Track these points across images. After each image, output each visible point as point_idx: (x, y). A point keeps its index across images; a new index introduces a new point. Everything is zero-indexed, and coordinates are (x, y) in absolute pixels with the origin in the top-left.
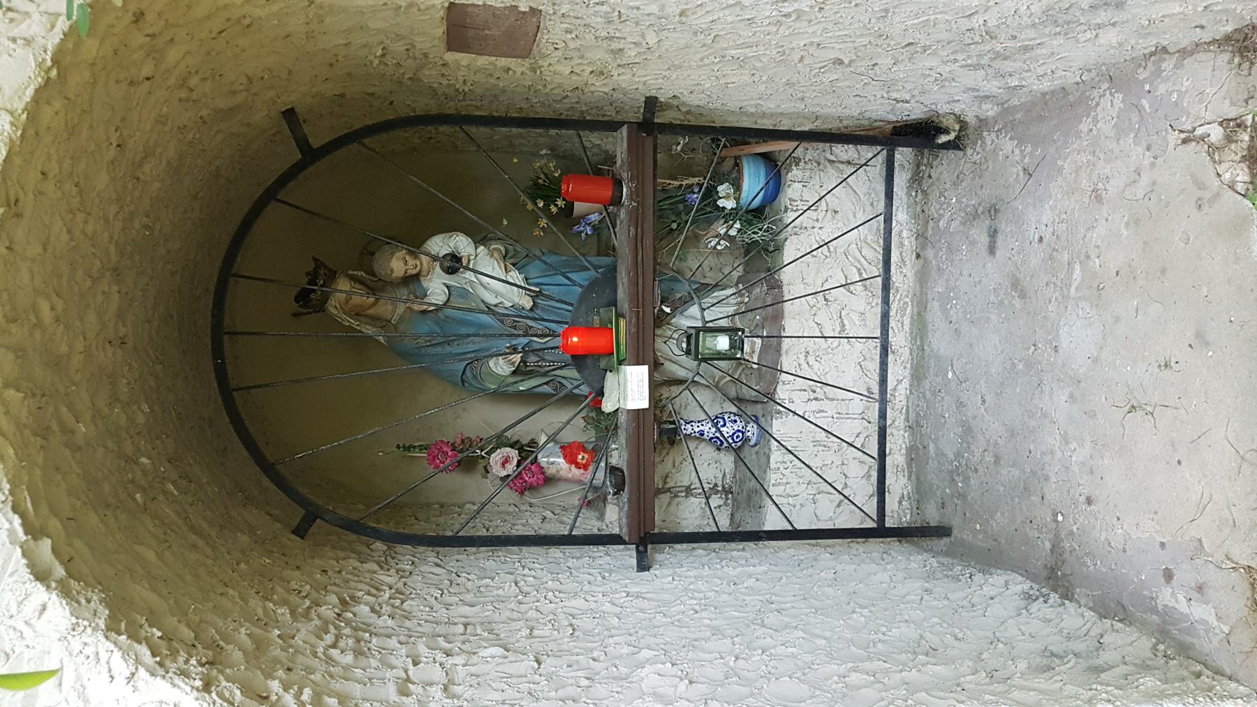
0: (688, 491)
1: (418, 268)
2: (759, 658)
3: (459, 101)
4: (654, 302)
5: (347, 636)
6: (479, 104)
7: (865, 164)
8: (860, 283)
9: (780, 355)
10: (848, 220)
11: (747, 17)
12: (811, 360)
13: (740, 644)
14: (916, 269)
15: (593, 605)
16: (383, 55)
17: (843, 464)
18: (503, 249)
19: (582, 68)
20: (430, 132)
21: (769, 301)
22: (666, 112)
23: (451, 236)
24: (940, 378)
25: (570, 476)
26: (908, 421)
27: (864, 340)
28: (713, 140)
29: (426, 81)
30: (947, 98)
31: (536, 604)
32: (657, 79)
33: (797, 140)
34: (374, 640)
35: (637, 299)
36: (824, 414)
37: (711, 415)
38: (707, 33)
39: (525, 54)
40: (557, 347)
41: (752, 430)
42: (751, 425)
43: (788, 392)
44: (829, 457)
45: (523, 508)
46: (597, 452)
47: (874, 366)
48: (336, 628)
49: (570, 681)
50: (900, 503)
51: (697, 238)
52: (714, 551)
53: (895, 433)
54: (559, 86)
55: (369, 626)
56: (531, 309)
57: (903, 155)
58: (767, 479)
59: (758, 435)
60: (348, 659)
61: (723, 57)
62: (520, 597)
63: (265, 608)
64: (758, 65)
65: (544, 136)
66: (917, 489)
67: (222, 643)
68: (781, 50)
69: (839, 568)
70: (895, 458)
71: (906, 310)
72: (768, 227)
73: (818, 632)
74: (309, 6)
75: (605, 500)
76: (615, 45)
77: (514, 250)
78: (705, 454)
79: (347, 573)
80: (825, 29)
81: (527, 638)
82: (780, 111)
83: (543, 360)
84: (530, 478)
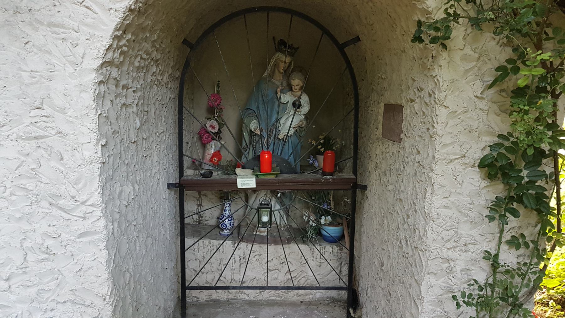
0: (200, 205)
1: (295, 91)
2: (135, 235)
3: (364, 108)
4: (282, 189)
5: (145, 63)
6: (363, 116)
7: (340, 278)
8: (290, 277)
9: (259, 244)
10: (317, 272)
11: (400, 226)
12: (257, 257)
13: (140, 227)
14: (296, 301)
15: (154, 165)
16: (382, 78)
17: (212, 272)
18: (303, 126)
19: (379, 159)
20: (351, 95)
21: (282, 239)
22: (361, 194)
23: (308, 104)
24: (250, 313)
25: (206, 154)
26: (231, 300)
27: (266, 280)
28: (350, 214)
29: (372, 95)
30: (368, 312)
31: (155, 141)
32: (374, 190)
33: (350, 249)
34: (143, 74)
35: (283, 182)
36: (234, 263)
37: (233, 215)
38: (393, 210)
39: (384, 136)
40: (263, 149)
41: (226, 232)
42: (229, 232)
43: (243, 247)
44: (215, 266)
45: (192, 134)
46: (217, 166)
47: (254, 284)
48: (148, 58)
49: (127, 156)
50: (195, 297)
51: (308, 208)
52: (175, 216)
53: (226, 294)
54: (371, 149)
55: (148, 72)
56: (278, 138)
57: (344, 294)
58: (206, 239)
59: (224, 235)
60: (137, 64)
61: (384, 217)
62: (158, 134)
63: (157, 30)
64: (381, 232)
65: (350, 143)
66: (202, 304)
67: (146, 15)
68: (387, 241)
69: (168, 270)
70: (215, 295)
71: (278, 297)
72: (313, 238)
73: (144, 260)
74: (401, 50)
75: (196, 169)
76: (388, 173)
77: (302, 131)
78: (216, 212)
79: (168, 61)
80: (396, 258)
81: (143, 137)
82: (362, 242)
83: (256, 143)
84: (205, 137)
